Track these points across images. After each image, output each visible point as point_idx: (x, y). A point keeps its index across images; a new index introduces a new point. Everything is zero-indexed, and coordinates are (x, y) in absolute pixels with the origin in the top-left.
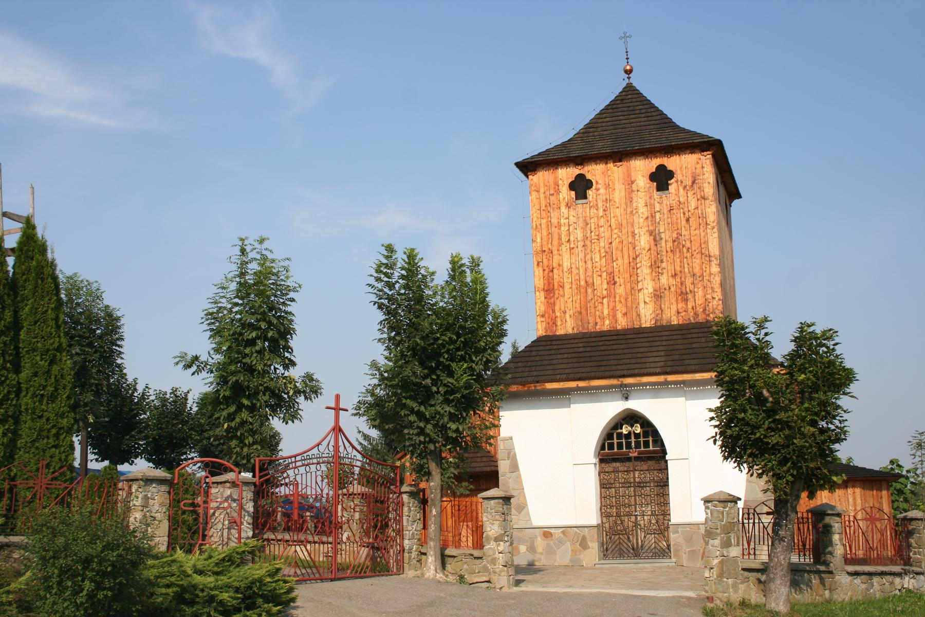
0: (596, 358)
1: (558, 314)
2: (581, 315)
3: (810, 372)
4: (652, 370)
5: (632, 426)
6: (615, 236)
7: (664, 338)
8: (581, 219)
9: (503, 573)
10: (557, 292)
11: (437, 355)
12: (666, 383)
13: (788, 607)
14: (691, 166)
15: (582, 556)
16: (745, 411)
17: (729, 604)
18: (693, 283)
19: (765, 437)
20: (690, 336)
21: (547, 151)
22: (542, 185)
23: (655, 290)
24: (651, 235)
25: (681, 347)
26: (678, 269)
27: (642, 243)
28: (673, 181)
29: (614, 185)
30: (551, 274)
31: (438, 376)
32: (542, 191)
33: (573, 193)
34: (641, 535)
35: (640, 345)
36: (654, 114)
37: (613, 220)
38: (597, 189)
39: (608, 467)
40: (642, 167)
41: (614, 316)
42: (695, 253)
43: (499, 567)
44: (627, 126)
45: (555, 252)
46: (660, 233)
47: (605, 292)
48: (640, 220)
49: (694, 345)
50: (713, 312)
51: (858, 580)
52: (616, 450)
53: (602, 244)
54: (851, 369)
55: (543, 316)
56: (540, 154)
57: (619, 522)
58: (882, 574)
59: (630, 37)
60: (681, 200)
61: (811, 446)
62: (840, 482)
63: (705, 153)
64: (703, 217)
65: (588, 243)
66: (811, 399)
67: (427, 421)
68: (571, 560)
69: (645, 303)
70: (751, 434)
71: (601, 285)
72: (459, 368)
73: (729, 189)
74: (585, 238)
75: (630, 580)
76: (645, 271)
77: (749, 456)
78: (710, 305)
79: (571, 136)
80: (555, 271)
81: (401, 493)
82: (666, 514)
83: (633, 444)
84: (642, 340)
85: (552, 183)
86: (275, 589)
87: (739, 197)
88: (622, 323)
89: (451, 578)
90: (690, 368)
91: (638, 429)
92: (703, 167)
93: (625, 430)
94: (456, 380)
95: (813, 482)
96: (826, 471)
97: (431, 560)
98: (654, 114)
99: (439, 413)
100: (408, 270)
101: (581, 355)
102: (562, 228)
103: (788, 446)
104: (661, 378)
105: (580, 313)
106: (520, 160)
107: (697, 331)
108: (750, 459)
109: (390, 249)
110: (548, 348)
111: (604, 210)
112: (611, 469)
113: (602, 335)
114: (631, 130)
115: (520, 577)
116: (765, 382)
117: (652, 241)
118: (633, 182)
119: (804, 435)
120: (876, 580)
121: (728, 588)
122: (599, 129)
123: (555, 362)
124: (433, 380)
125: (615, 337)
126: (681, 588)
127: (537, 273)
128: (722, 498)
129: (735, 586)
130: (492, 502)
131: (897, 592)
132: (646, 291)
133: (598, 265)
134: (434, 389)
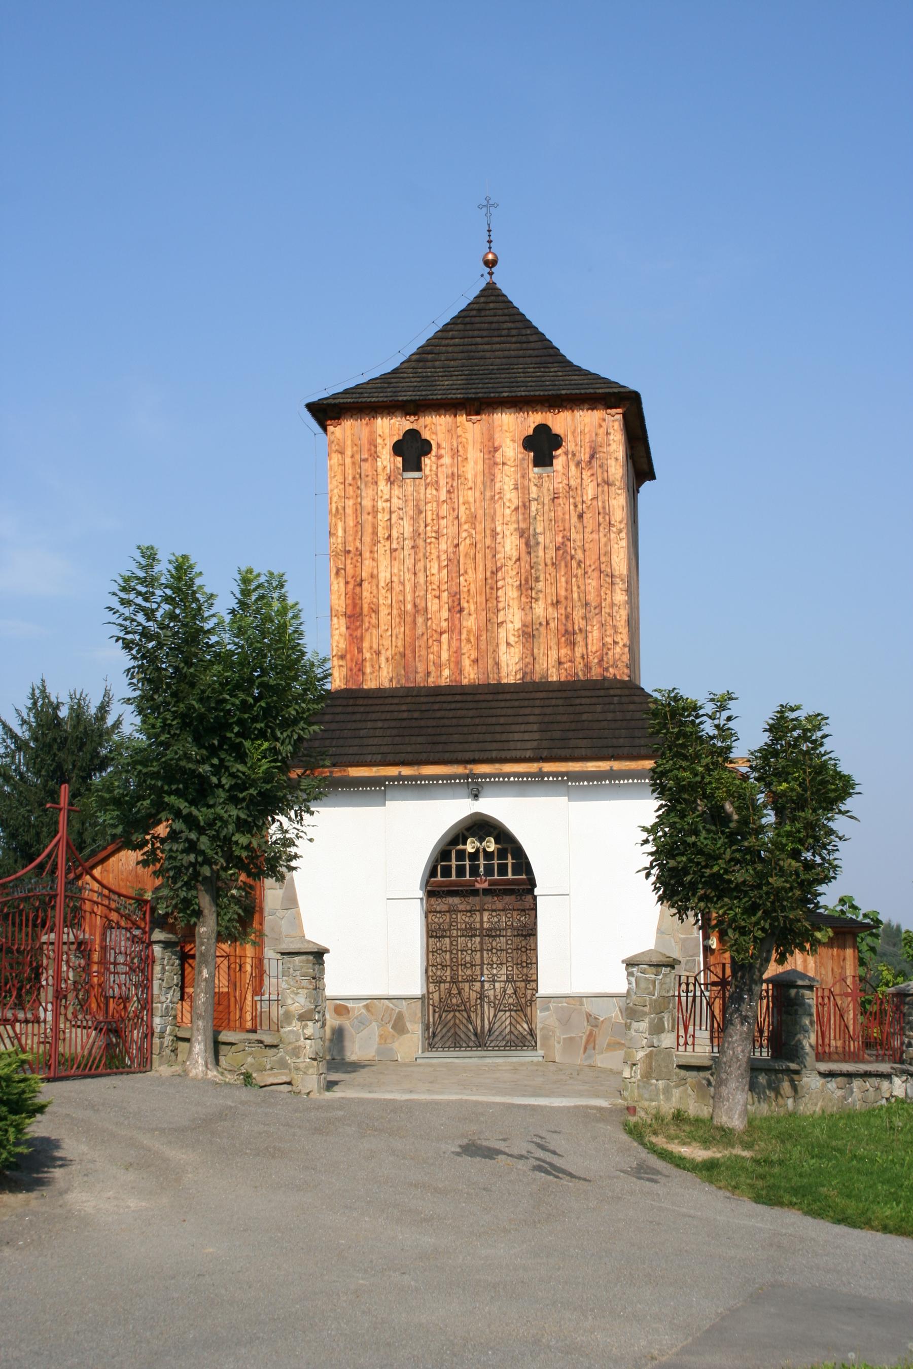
0: (430, 731)
1: (367, 655)
2: (404, 658)
3: (796, 779)
4: (518, 754)
5: (481, 840)
6: (464, 535)
7: (538, 703)
8: (411, 504)
9: (311, 1071)
10: (366, 619)
11: (222, 726)
12: (541, 774)
13: (745, 1122)
14: (589, 430)
15: (395, 1046)
16: (696, 833)
17: (658, 1117)
18: (585, 618)
19: (726, 871)
20: (578, 701)
21: (357, 387)
22: (349, 442)
23: (524, 625)
24: (521, 536)
25: (564, 718)
26: (562, 593)
27: (508, 548)
28: (559, 452)
29: (466, 450)
30: (358, 589)
31: (222, 761)
32: (349, 452)
33: (400, 459)
34: (489, 1012)
35: (499, 712)
36: (532, 338)
37: (462, 509)
38: (439, 457)
39: (441, 904)
40: (511, 426)
41: (458, 663)
42: (590, 570)
43: (304, 1060)
44: (488, 355)
45: (367, 555)
46: (535, 534)
47: (444, 624)
48: (505, 512)
49: (584, 717)
50: (615, 665)
51: (832, 1085)
52: (454, 878)
53: (443, 546)
54: (849, 776)
55: (342, 657)
56: (346, 392)
57: (455, 991)
58: (866, 1075)
59: (495, 206)
60: (572, 483)
61: (791, 889)
62: (825, 940)
63: (613, 411)
64: (605, 512)
65: (421, 543)
66: (793, 820)
67: (201, 831)
68: (379, 1052)
69: (508, 644)
70: (706, 867)
71: (439, 611)
72: (256, 748)
73: (641, 469)
74: (416, 534)
75: (475, 1083)
76: (509, 593)
77: (701, 899)
78: (610, 653)
79: (397, 364)
80: (365, 585)
81: (151, 943)
82: (531, 980)
83: (482, 869)
84: (502, 704)
85: (365, 441)
86: (24, 1092)
87: (652, 477)
88: (470, 675)
89: (230, 1078)
90: (577, 753)
91: (491, 846)
92: (608, 434)
93: (470, 848)
94: (249, 768)
95: (787, 938)
96: (807, 924)
97: (199, 1048)
98: (532, 338)
99: (221, 818)
100: (177, 590)
101: (404, 724)
102: (380, 516)
103: (759, 887)
104: (533, 767)
105: (404, 655)
106: (314, 399)
107: (588, 693)
108: (702, 904)
109: (150, 555)
110: (350, 709)
111: (449, 492)
112: (445, 908)
113: (437, 692)
114: (490, 361)
115: (334, 1077)
116: (728, 791)
117: (523, 546)
118: (496, 450)
119: (782, 872)
120: (857, 1083)
121: (657, 1095)
122: (443, 357)
123: (362, 733)
124: (212, 765)
125: (458, 698)
126: (580, 1094)
127: (335, 587)
128: (655, 959)
129: (667, 1091)
130: (297, 959)
131: (884, 1102)
132: (510, 626)
133: (435, 579)
134: (214, 780)
